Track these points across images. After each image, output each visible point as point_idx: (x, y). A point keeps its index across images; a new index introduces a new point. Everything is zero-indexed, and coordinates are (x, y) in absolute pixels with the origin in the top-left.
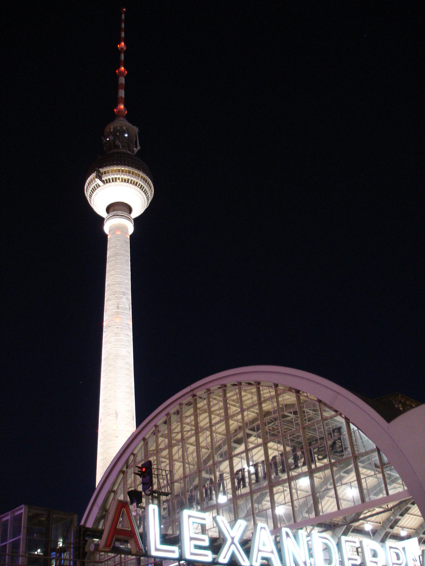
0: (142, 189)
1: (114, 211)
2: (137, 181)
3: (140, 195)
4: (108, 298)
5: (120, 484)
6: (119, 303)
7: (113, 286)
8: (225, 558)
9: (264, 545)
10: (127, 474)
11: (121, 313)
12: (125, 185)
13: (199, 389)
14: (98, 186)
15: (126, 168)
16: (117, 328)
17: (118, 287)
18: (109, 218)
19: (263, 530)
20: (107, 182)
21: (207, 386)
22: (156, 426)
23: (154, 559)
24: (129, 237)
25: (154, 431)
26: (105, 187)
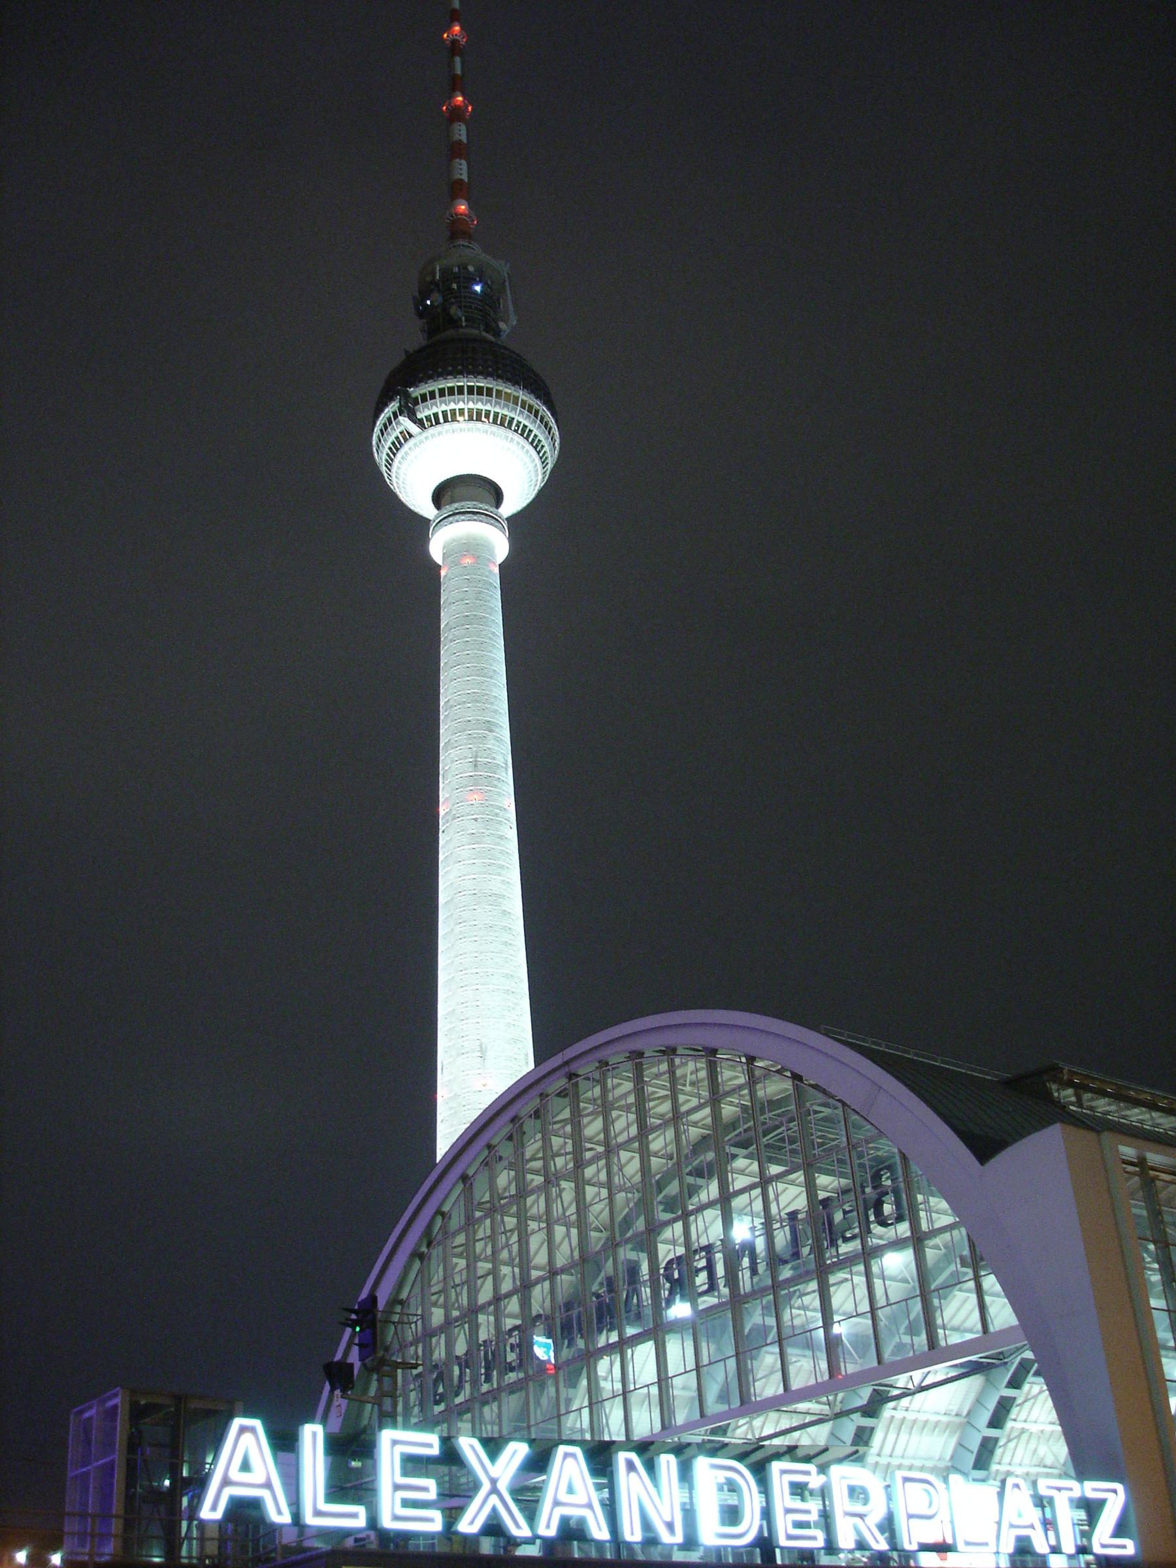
0: (525, 435)
1: (453, 501)
2: (513, 416)
4: (447, 741)
5: (415, 1284)
6: (476, 752)
8: (472, 1522)
9: (570, 1490)
12: (479, 429)
13: (582, 1061)
16: (476, 820)
18: (441, 523)
19: (570, 1460)
21: (600, 1054)
22: (489, 1147)
24: (496, 570)
25: (486, 1158)
26: (426, 438)
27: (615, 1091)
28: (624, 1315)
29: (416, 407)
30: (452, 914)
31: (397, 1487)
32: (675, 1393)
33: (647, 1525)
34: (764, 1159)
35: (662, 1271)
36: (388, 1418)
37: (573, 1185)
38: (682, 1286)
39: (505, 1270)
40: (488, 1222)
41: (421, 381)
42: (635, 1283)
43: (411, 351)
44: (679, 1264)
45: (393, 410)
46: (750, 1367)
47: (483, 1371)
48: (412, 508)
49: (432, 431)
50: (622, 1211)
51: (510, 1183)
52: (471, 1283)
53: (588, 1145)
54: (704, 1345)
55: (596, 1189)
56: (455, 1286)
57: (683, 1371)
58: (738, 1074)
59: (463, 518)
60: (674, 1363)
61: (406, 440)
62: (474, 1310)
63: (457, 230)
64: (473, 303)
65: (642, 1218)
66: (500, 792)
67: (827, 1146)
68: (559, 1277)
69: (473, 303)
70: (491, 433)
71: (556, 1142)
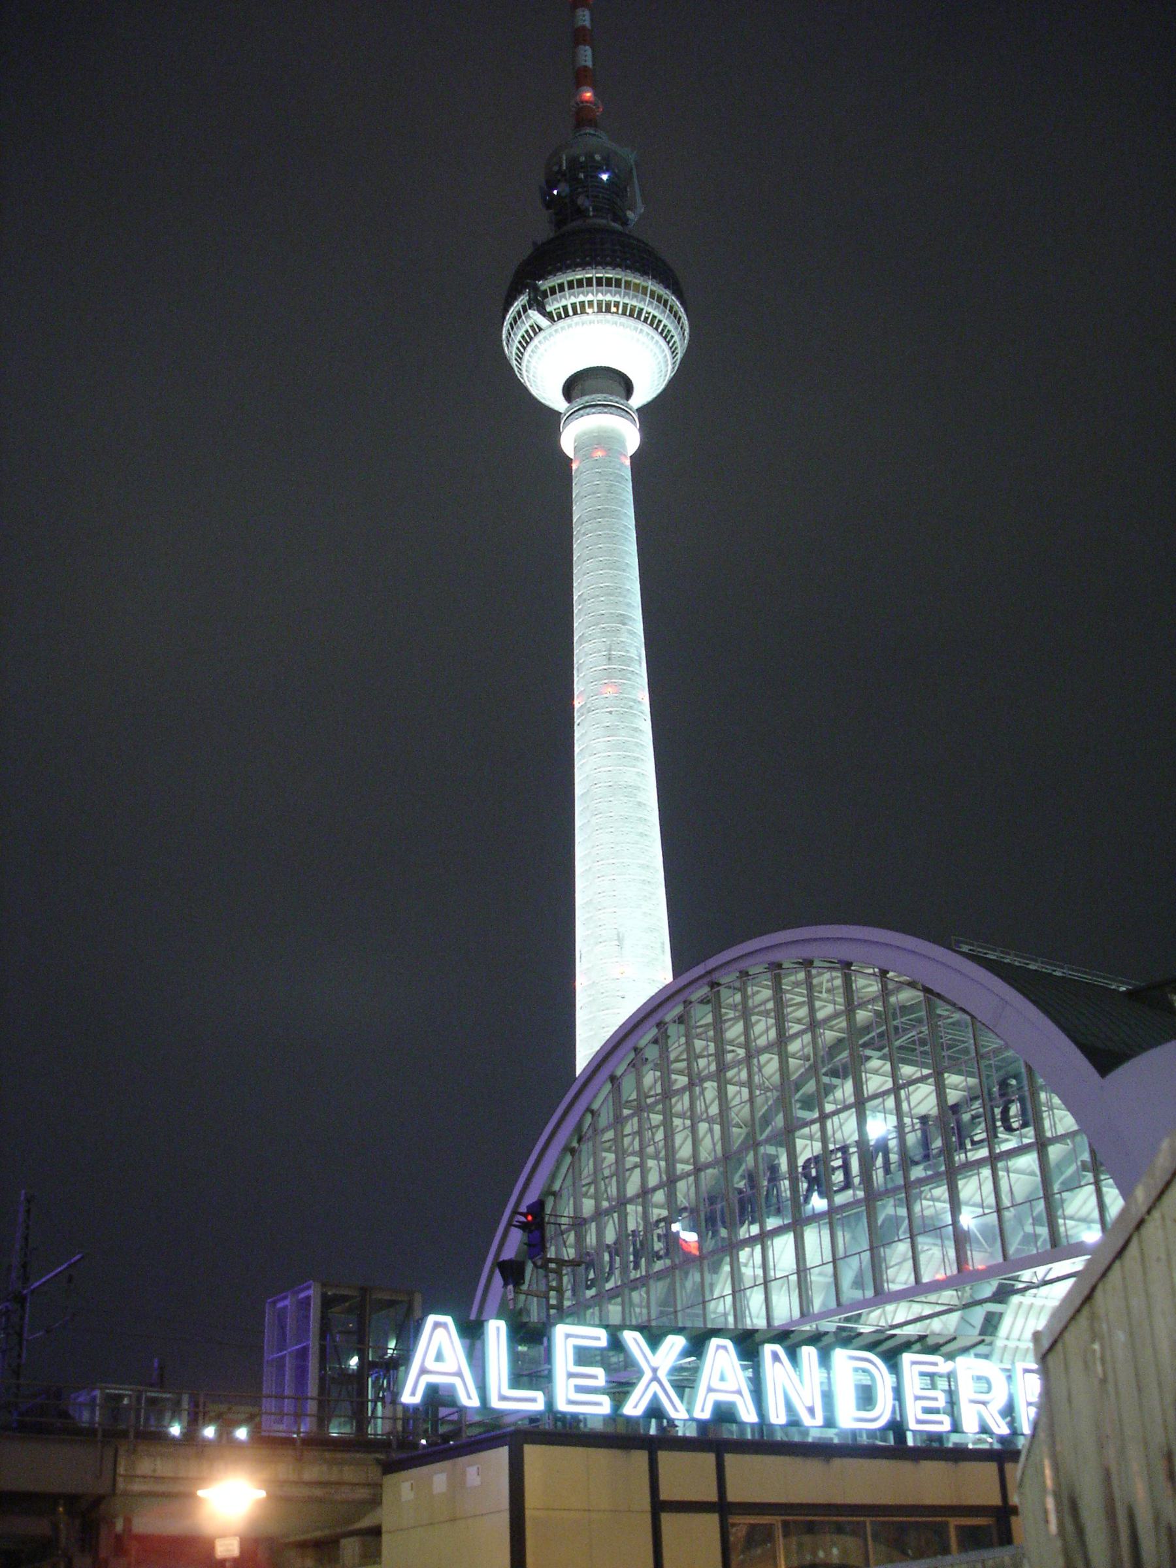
0: (654, 326)
1: (583, 394)
2: (642, 306)
3: (651, 344)
7: (593, 602)
8: (635, 1407)
9: (722, 1379)
10: (580, 1154)
11: (619, 673)
14: (537, 329)
15: (608, 273)
16: (610, 712)
17: (607, 604)
19: (721, 1351)
20: (560, 318)
21: (742, 965)
22: (636, 1049)
23: (571, 1379)
24: (628, 462)
26: (556, 331)
27: (755, 997)
28: (764, 1210)
29: (546, 300)
30: (588, 806)
31: (571, 1375)
32: (813, 1278)
33: (790, 1408)
34: (896, 1061)
35: (800, 1170)
36: (563, 1314)
37: (715, 1084)
38: (820, 1183)
39: (651, 1163)
40: (635, 1119)
41: (550, 273)
42: (776, 1180)
43: (540, 243)
44: (816, 1163)
45: (522, 303)
46: (882, 1254)
47: (631, 1258)
48: (543, 401)
49: (561, 323)
50: (761, 1108)
51: (655, 1082)
52: (620, 1173)
53: (729, 1048)
54: (840, 1234)
55: (737, 1088)
56: (604, 1179)
57: (821, 1263)
58: (870, 982)
59: (593, 410)
60: (813, 1256)
61: (536, 334)
62: (622, 1202)
63: (583, 118)
64: (600, 192)
65: (781, 1116)
66: (634, 685)
67: (957, 1048)
68: (703, 1173)
69: (600, 192)
70: (620, 325)
71: (699, 1044)
